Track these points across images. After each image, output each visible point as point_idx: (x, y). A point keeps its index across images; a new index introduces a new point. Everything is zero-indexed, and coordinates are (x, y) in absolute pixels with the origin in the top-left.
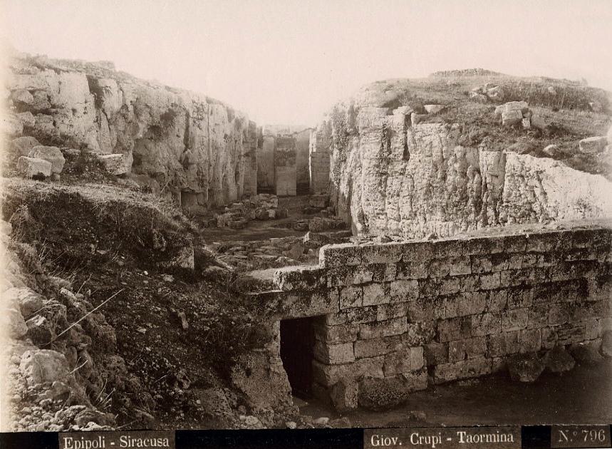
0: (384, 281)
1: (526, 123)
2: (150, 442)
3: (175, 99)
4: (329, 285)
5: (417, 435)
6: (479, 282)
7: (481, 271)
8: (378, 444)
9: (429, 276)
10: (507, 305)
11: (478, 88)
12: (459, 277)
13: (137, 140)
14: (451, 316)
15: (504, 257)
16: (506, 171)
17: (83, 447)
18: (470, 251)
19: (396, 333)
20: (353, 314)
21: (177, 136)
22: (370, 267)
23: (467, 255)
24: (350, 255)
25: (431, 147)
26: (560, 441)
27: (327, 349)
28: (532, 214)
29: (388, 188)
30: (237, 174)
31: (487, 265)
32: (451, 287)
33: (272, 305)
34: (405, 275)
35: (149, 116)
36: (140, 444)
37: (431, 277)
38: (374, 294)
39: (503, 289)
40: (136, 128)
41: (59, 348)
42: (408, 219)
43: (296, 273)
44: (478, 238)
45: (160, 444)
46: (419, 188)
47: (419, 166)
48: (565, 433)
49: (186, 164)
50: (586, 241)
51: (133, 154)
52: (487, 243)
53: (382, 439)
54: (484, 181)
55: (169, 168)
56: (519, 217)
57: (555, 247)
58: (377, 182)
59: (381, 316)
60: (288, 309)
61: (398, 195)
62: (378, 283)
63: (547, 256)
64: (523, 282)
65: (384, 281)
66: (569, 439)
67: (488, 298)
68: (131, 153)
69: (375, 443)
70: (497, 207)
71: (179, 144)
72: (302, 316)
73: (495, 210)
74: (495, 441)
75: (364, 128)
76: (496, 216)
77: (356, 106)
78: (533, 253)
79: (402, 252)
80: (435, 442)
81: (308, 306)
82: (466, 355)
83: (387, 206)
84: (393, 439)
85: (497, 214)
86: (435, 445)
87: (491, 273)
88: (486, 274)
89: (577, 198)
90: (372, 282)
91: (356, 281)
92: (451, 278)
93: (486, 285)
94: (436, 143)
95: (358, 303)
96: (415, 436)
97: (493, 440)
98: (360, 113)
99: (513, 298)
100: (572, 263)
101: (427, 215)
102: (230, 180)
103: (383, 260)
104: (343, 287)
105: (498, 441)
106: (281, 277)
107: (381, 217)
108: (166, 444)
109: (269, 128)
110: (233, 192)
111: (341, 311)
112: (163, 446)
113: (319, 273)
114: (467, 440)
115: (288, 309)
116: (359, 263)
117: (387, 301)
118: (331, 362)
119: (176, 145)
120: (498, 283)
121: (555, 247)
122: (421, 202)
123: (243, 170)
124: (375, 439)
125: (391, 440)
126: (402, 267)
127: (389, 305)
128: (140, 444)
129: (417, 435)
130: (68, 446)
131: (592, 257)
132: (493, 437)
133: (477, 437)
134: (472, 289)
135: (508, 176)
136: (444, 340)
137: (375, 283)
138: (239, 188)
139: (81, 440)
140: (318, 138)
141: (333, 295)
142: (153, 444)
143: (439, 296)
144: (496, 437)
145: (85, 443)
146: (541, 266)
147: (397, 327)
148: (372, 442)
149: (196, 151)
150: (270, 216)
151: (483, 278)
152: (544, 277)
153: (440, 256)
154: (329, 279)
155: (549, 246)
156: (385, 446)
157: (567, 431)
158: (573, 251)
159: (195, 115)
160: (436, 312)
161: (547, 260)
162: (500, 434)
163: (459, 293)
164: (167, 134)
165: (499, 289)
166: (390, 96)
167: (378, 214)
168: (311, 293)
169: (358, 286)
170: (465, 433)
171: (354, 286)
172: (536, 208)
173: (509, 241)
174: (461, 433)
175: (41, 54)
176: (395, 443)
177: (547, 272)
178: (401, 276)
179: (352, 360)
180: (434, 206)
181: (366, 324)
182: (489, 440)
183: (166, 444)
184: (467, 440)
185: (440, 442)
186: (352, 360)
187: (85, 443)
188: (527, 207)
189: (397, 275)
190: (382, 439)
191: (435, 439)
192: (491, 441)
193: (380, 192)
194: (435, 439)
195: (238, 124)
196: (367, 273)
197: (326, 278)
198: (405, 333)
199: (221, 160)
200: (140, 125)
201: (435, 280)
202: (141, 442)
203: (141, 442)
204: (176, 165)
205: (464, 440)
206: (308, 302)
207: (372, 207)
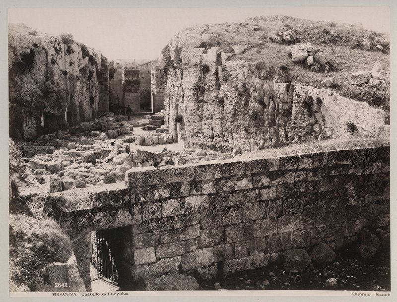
0: (179, 196)
1: (310, 60)
3: (35, 39)
4: (133, 201)
6: (260, 195)
7: (261, 186)
9: (217, 191)
10: (282, 211)
11: (276, 32)
12: (242, 191)
14: (236, 222)
15: (281, 173)
16: (294, 99)
18: (252, 170)
19: (191, 238)
20: (154, 224)
22: (168, 186)
23: (249, 173)
24: (151, 177)
25: (237, 80)
27: (133, 253)
28: (313, 134)
29: (204, 112)
31: (265, 181)
32: (233, 200)
33: (84, 220)
34: (197, 191)
37: (220, 192)
38: (169, 208)
39: (279, 199)
43: (105, 193)
44: (258, 159)
46: (228, 112)
47: (147, 134)
50: (346, 159)
52: (265, 163)
54: (277, 107)
56: (304, 136)
57: (321, 164)
58: (196, 107)
59: (178, 225)
60: (98, 222)
61: (212, 118)
62: (175, 198)
63: (315, 171)
64: (296, 193)
65: (179, 196)
67: (266, 206)
70: (287, 128)
71: (40, 76)
72: (111, 228)
73: (285, 129)
75: (185, 64)
76: (286, 135)
77: (179, 46)
78: (303, 170)
79: (195, 172)
81: (115, 220)
82: (249, 253)
83: (204, 126)
85: (286, 133)
87: (269, 187)
88: (265, 188)
89: (347, 121)
90: (169, 198)
91: (156, 198)
92: (236, 192)
93: (265, 197)
94: (240, 76)
95: (158, 215)
98: (182, 52)
99: (287, 205)
100: (335, 177)
101: (234, 134)
102: (86, 103)
103: (179, 179)
104: (145, 203)
106: (92, 197)
107: (199, 135)
109: (118, 62)
110: (87, 110)
111: (143, 222)
113: (124, 192)
115: (98, 222)
116: (159, 183)
117: (182, 212)
118: (136, 263)
120: (275, 194)
121: (321, 164)
122: (229, 124)
123: (97, 94)
126: (195, 185)
131: (351, 172)
134: (254, 200)
135: (295, 103)
136: (231, 241)
137: (172, 198)
138: (93, 110)
140: (157, 70)
141: (136, 210)
143: (226, 207)
146: (310, 179)
147: (194, 232)
151: (262, 191)
152: (312, 189)
153: (226, 175)
154: (133, 196)
155: (317, 164)
158: (335, 167)
160: (224, 219)
161: (315, 175)
163: (243, 203)
165: (275, 199)
166: (205, 38)
167: (196, 132)
168: (117, 209)
169: (157, 201)
171: (155, 201)
172: (317, 129)
173: (285, 160)
177: (315, 184)
178: (194, 192)
179: (154, 260)
180: (239, 127)
181: (165, 231)
186: (154, 260)
188: (310, 127)
189: (190, 191)
193: (199, 115)
195: (92, 60)
196: (166, 191)
197: (130, 195)
201: (223, 194)
206: (115, 216)
207: (192, 127)
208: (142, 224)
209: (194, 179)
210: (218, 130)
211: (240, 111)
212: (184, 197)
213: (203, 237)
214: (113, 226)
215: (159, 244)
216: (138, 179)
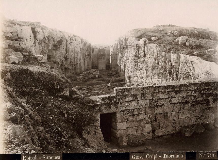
0: (137, 100)
1: (187, 44)
2: (53, 158)
3: (62, 35)
4: (117, 101)
5: (149, 155)
6: (171, 101)
7: (172, 97)
8: (135, 158)
9: (153, 98)
10: (180, 109)
12: (163, 99)
13: (49, 50)
14: (161, 113)
15: (180, 91)
16: (180, 61)
17: (30, 159)
18: (168, 90)
19: (141, 119)
20: (126, 112)
21: (63, 48)
22: (132, 95)
23: (166, 91)
24: (125, 91)
25: (154, 53)
26: (200, 157)
27: (117, 124)
28: (190, 76)
29: (138, 67)
30: (84, 62)
31: (173, 95)
33: (97, 109)
34: (144, 98)
35: (53, 41)
36: (50, 158)
37: (154, 99)
38: (133, 105)
39: (179, 103)
40: (49, 46)
41: (21, 124)
42: (146, 78)
43: (106, 97)
44: (170, 85)
45: (57, 158)
46: (149, 67)
47: (149, 59)
48: (201, 154)
49: (66, 58)
50: (209, 86)
51: (47, 55)
52: (173, 87)
53: (136, 157)
54: (172, 64)
55: (60, 60)
56: (185, 77)
57: (198, 88)
58: (134, 65)
59: (136, 113)
60: (103, 110)
61: (142, 70)
62: (135, 101)
63: (195, 91)
64: (186, 101)
65: (137, 100)
66: (203, 157)
67: (174, 106)
68: (47, 54)
69: (134, 158)
70: (177, 74)
72: (108, 113)
73: (176, 75)
74: (176, 157)
75: (130, 46)
77: (127, 38)
78: (190, 90)
79: (143, 90)
80: (155, 158)
81: (110, 109)
82: (166, 127)
83: (138, 73)
84: (140, 156)
85: (177, 76)
86: (155, 159)
87: (175, 97)
88: (173, 98)
89: (205, 70)
90: (132, 101)
91: (127, 100)
92: (161, 99)
94: (155, 51)
95: (128, 108)
96: (148, 155)
97: (175, 157)
98: (128, 40)
99: (183, 106)
100: (204, 94)
102: (82, 64)
103: (136, 93)
104: (122, 102)
105: (177, 157)
106: (100, 99)
107: (136, 77)
108: (59, 158)
109: (96, 46)
110: (83, 69)
111: (121, 111)
112: (58, 159)
113: (114, 97)
114: (166, 157)
115: (103, 110)
116: (128, 94)
117: (138, 107)
118: (118, 129)
119: (63, 52)
120: (177, 101)
121: (198, 88)
122: (150, 72)
123: (87, 61)
124: (134, 156)
125: (139, 157)
126: (143, 95)
127: (139, 109)
128: (50, 158)
129: (149, 155)
130: (24, 159)
131: (211, 92)
132: (176, 156)
133: (170, 156)
134: (168, 103)
135: (181, 63)
136: (158, 121)
137: (134, 101)
138: (85, 67)
139: (29, 157)
140: (113, 49)
141: (118, 105)
142: (55, 158)
144: (177, 156)
145: (30, 158)
146: (193, 95)
148: (133, 158)
149: (70, 54)
150: (96, 77)
151: (172, 99)
152: (194, 99)
153: (157, 91)
154: (117, 99)
155: (196, 88)
156: (137, 159)
157: (202, 154)
158: (204, 89)
159: (70, 41)
160: (155, 111)
161: (195, 93)
162: (178, 155)
163: (163, 104)
164: (59, 48)
165: (178, 103)
166: (139, 34)
167: (135, 76)
168: (111, 104)
169: (127, 102)
170: (166, 154)
171: (126, 102)
172: (191, 74)
173: (181, 86)
174: (164, 154)
175: (15, 19)
176: (141, 158)
177: (195, 97)
178: (143, 98)
179: (126, 128)
180: (154, 73)
181: (130, 115)
182: (174, 157)
183: (59, 158)
184: (166, 157)
185: (157, 158)
186: (126, 128)
187: (30, 158)
188: (188, 74)
189: (141, 98)
190: (136, 157)
191: (155, 156)
192: (175, 157)
193: (135, 68)
194: (155, 156)
195: (85, 44)
196: (131, 97)
197: (116, 99)
198: (144, 119)
199: (79, 57)
200: (50, 44)
201: (155, 100)
202: (50, 158)
203: (50, 158)
204: (63, 59)
205: (165, 157)
206: (110, 108)
207: (132, 74)
208: (121, 112)
209: (143, 93)
210: (145, 75)
211: (155, 67)
212: (139, 101)
213: (146, 118)
214: (109, 112)
215: (127, 121)
216: (120, 92)
